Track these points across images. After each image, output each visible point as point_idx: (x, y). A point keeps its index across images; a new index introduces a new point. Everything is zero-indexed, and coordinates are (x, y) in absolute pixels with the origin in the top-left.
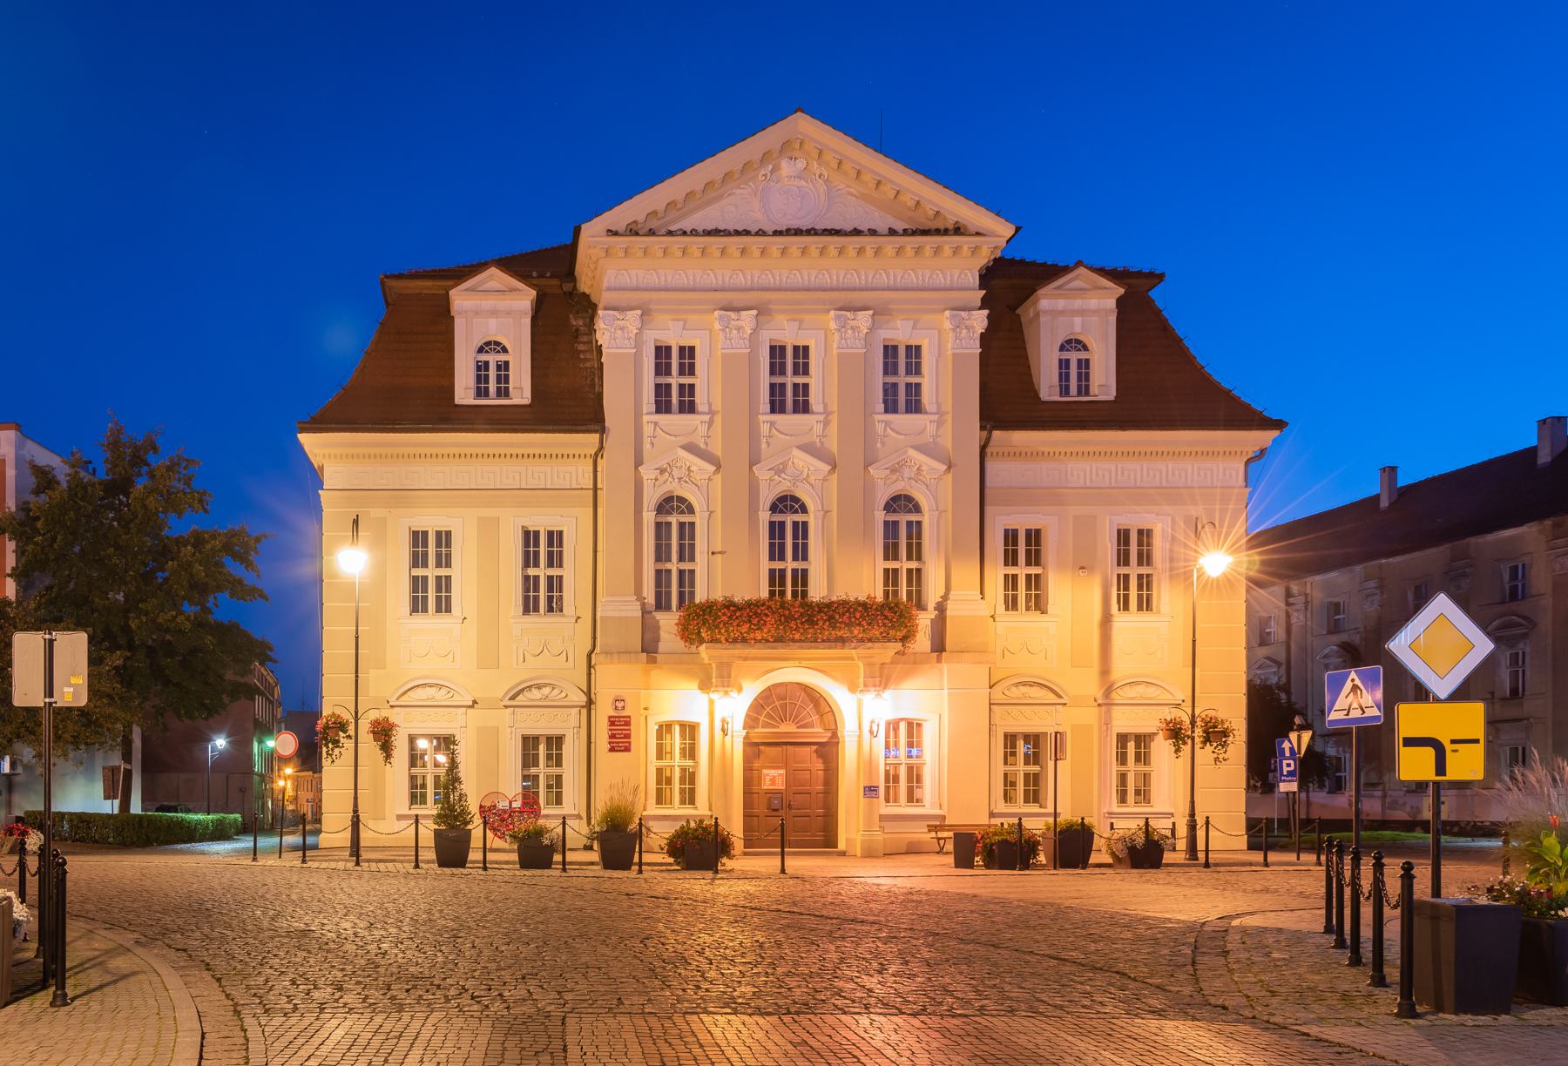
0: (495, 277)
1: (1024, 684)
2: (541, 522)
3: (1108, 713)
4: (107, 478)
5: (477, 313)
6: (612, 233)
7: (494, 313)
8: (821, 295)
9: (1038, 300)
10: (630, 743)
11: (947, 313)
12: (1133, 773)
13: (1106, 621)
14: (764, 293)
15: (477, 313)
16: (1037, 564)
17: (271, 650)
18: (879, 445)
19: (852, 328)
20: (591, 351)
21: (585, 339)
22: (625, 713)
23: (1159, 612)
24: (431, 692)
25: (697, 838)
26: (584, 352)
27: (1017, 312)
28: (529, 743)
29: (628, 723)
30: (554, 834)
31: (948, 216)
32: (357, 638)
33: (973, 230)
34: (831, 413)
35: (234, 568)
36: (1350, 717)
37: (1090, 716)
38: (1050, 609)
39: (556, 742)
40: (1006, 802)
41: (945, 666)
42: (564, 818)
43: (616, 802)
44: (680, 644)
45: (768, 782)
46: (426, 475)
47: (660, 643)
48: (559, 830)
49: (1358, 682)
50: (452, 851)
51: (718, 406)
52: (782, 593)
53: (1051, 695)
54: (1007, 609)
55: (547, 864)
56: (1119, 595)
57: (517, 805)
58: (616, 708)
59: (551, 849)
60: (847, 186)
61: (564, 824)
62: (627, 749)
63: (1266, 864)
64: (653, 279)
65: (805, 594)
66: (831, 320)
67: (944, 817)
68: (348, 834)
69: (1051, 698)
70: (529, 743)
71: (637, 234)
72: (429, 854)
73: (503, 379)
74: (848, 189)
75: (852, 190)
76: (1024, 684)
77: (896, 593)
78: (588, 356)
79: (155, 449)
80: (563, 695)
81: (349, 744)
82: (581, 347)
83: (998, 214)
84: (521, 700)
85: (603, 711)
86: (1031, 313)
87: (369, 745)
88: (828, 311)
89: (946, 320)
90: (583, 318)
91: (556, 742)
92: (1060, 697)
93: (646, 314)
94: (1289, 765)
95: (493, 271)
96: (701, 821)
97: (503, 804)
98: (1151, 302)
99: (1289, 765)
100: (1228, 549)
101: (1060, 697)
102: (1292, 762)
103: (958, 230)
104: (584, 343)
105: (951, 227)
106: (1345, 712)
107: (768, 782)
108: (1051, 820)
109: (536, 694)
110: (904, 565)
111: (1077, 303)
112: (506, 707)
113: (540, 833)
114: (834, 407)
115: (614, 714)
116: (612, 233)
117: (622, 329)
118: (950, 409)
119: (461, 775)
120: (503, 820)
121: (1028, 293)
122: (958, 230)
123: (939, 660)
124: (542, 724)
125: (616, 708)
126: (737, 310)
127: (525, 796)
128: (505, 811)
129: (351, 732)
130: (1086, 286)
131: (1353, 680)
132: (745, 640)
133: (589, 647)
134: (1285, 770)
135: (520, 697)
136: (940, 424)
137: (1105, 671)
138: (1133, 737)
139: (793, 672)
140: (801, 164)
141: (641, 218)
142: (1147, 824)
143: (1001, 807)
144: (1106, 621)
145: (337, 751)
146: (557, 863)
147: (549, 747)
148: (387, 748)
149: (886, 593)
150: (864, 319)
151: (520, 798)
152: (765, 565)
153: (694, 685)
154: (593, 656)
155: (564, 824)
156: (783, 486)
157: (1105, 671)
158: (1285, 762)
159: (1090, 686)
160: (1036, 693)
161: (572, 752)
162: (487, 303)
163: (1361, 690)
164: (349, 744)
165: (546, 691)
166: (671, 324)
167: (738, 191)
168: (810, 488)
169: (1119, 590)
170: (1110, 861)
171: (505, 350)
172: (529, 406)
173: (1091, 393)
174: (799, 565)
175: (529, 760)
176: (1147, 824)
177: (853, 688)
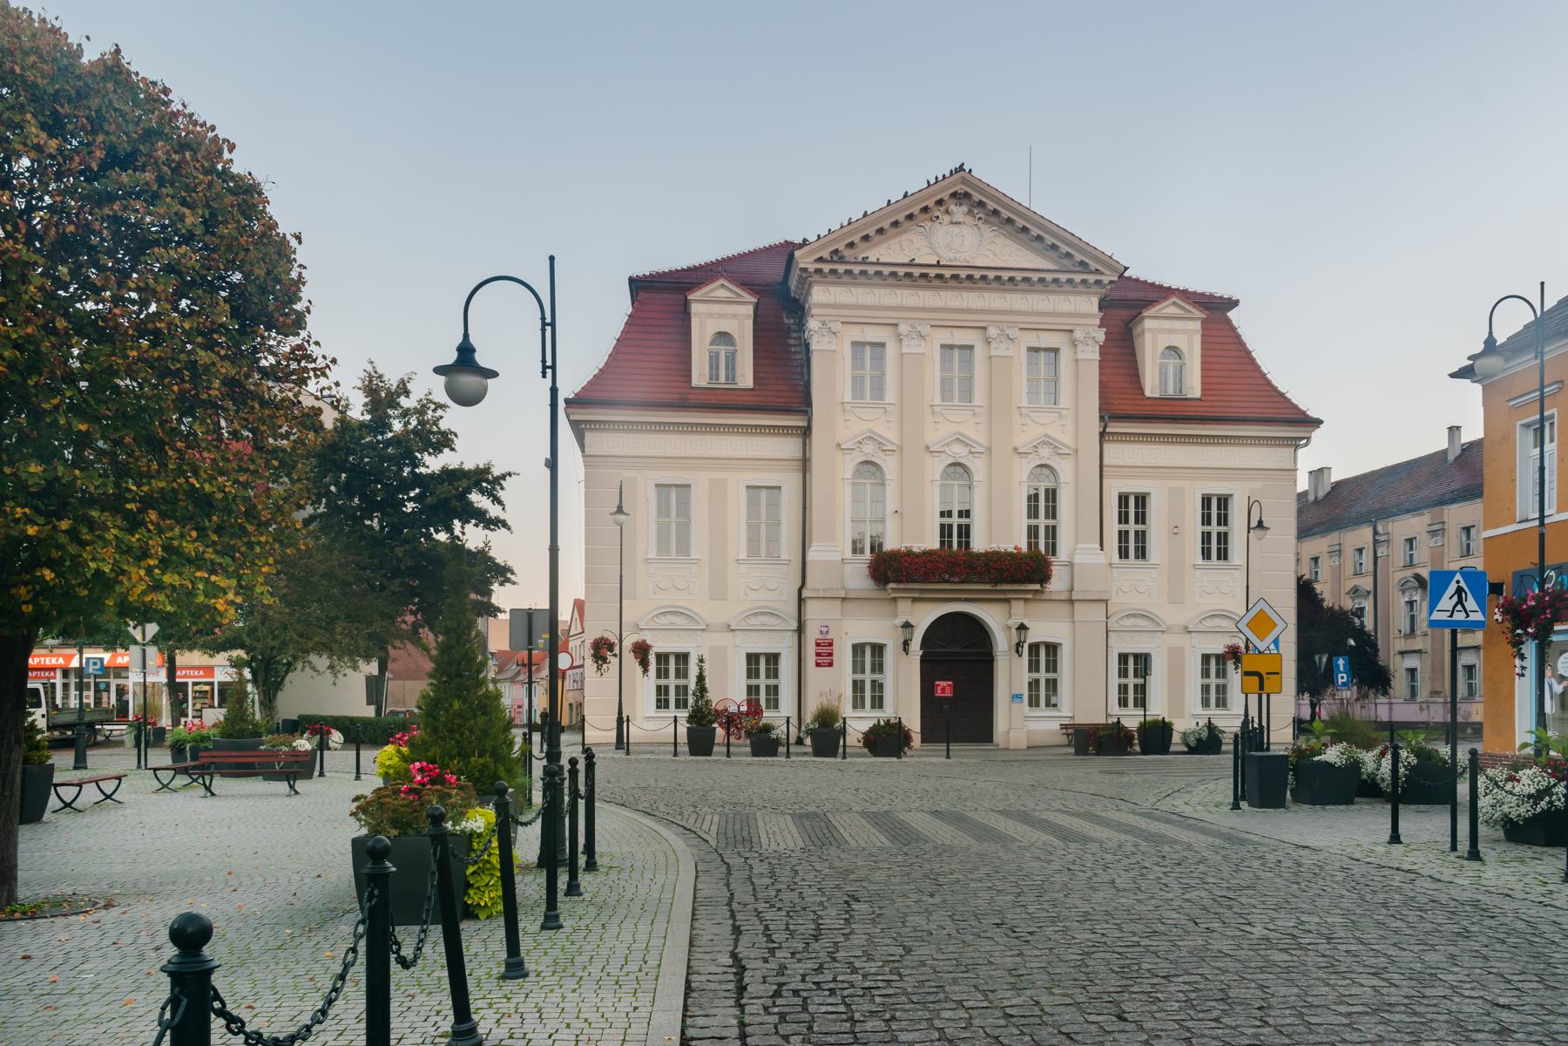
1: (1133, 615)
4: (361, 418)
17: (513, 573)
20: (800, 345)
21: (795, 335)
22: (829, 636)
24: (672, 618)
25: (885, 733)
28: (752, 659)
29: (831, 644)
30: (779, 731)
35: (477, 499)
36: (1477, 609)
39: (773, 659)
40: (1120, 706)
43: (825, 706)
45: (939, 691)
48: (784, 728)
49: (1463, 584)
50: (700, 743)
52: (950, 543)
54: (1121, 557)
55: (774, 753)
57: (744, 709)
58: (821, 632)
59: (777, 742)
62: (831, 665)
65: (968, 544)
68: (614, 733)
70: (752, 659)
72: (684, 748)
76: (1133, 615)
77: (1037, 544)
78: (798, 349)
79: (407, 393)
81: (614, 661)
82: (792, 342)
85: (812, 635)
86: (1139, 330)
87: (630, 660)
91: (773, 659)
94: (1342, 678)
96: (889, 721)
97: (733, 709)
98: (1229, 322)
99: (1342, 678)
102: (1345, 675)
104: (795, 338)
106: (1449, 614)
108: (1142, 719)
113: (768, 729)
119: (707, 685)
121: (1136, 317)
124: (762, 646)
125: (821, 632)
127: (749, 702)
129: (617, 651)
131: (1458, 582)
133: (799, 584)
134: (1340, 681)
142: (1209, 721)
143: (1115, 709)
145: (605, 666)
146: (782, 754)
147: (768, 663)
148: (644, 664)
149: (1029, 544)
151: (745, 703)
154: (803, 591)
158: (1340, 675)
160: (1142, 623)
161: (787, 667)
163: (1466, 593)
164: (614, 661)
170: (1186, 749)
175: (752, 673)
176: (1209, 721)
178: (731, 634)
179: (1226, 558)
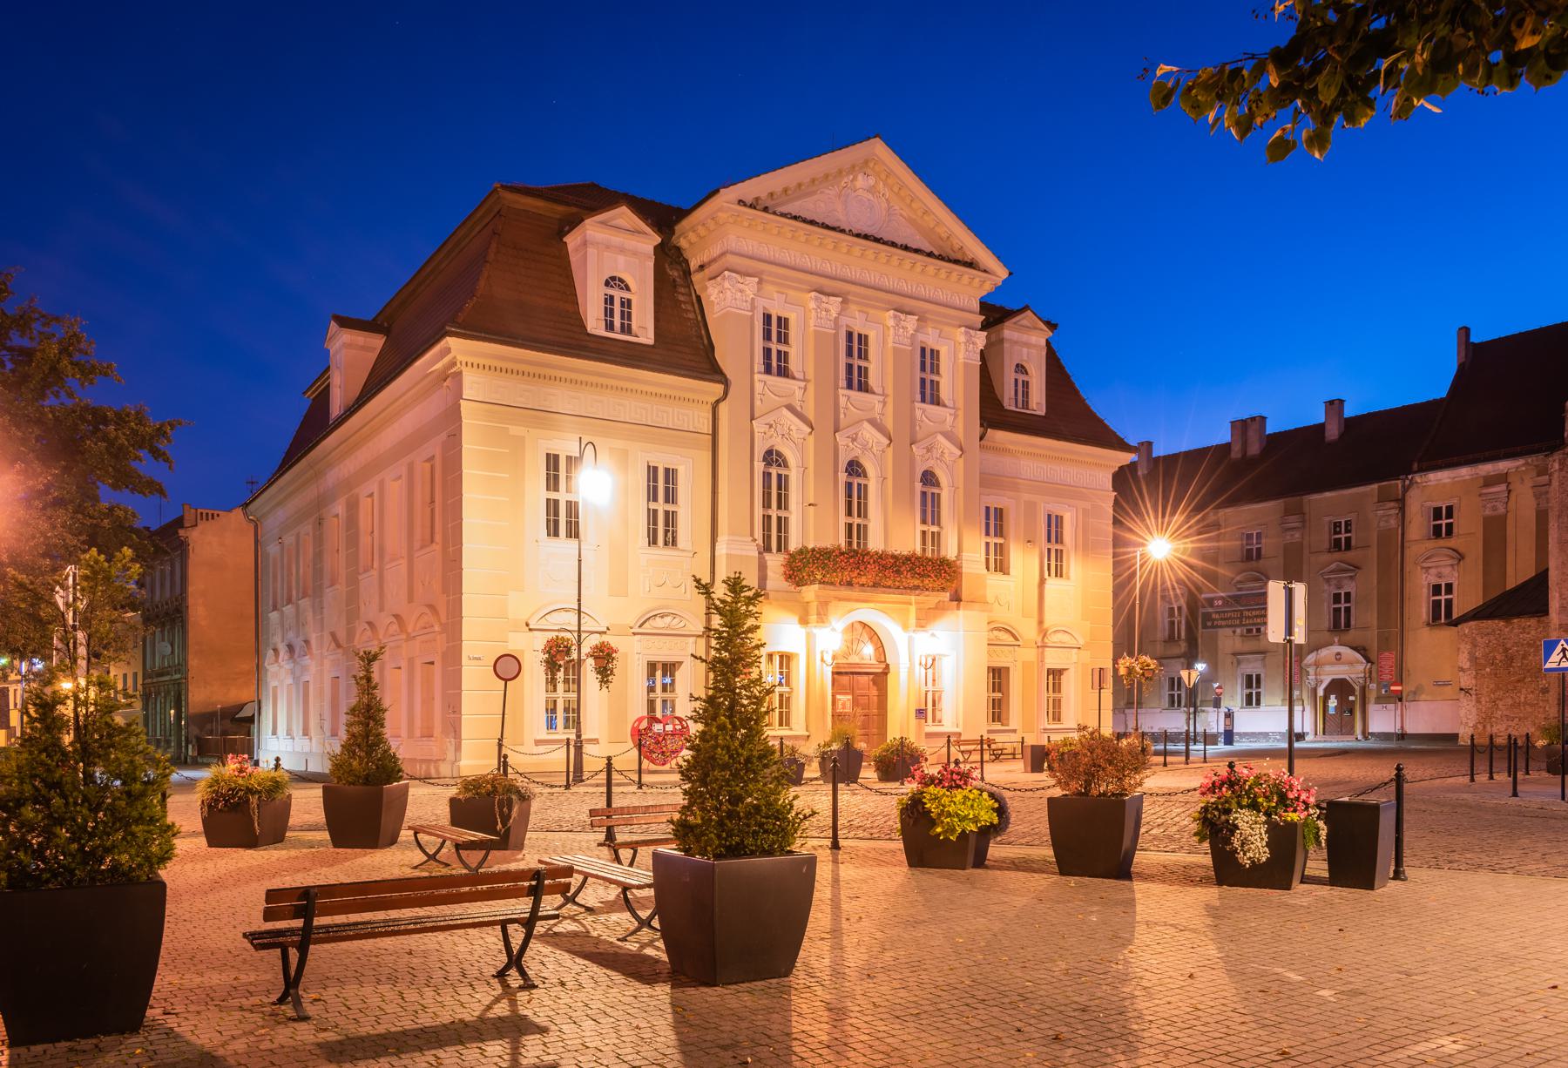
0: (623, 215)
2: (662, 461)
3: (1043, 653)
5: (608, 247)
6: (741, 202)
7: (622, 250)
8: (953, 312)
9: (1003, 329)
11: (963, 329)
13: (1042, 582)
15: (608, 247)
18: (918, 428)
19: (903, 328)
23: (1068, 578)
26: (685, 303)
27: (565, 240)
31: (968, 253)
32: (580, 561)
33: (982, 267)
34: (887, 396)
37: (1030, 654)
38: (1012, 571)
41: (961, 612)
42: (782, 739)
44: (785, 585)
45: (840, 706)
46: (561, 399)
47: (768, 582)
51: (811, 375)
53: (1012, 639)
56: (996, 560)
63: (1165, 764)
64: (765, 251)
65: (865, 544)
66: (889, 318)
67: (960, 734)
69: (1011, 640)
71: (755, 208)
73: (627, 316)
75: (904, 214)
80: (682, 624)
83: (999, 258)
84: (647, 628)
88: (888, 310)
89: (960, 335)
90: (677, 270)
92: (1017, 639)
93: (845, 302)
95: (624, 209)
101: (1017, 639)
103: (971, 265)
107: (840, 706)
109: (659, 622)
110: (856, 521)
111: (1025, 338)
112: (634, 634)
114: (890, 391)
116: (741, 202)
117: (741, 291)
118: (962, 408)
120: (658, 742)
122: (971, 265)
123: (958, 608)
124: (664, 651)
126: (829, 295)
128: (659, 734)
130: (1029, 325)
132: (850, 584)
135: (647, 625)
136: (956, 416)
137: (1041, 622)
138: (661, 666)
139: (867, 613)
140: (872, 181)
141: (763, 195)
144: (1042, 582)
150: (911, 322)
152: (843, 519)
153: (795, 619)
156: (856, 452)
157: (1041, 622)
159: (1028, 630)
162: (617, 239)
165: (668, 620)
166: (775, 295)
167: (827, 191)
168: (945, 467)
169: (996, 555)
171: (628, 289)
172: (653, 346)
173: (1030, 407)
174: (653, 506)
177: (905, 627)
178: (531, 634)
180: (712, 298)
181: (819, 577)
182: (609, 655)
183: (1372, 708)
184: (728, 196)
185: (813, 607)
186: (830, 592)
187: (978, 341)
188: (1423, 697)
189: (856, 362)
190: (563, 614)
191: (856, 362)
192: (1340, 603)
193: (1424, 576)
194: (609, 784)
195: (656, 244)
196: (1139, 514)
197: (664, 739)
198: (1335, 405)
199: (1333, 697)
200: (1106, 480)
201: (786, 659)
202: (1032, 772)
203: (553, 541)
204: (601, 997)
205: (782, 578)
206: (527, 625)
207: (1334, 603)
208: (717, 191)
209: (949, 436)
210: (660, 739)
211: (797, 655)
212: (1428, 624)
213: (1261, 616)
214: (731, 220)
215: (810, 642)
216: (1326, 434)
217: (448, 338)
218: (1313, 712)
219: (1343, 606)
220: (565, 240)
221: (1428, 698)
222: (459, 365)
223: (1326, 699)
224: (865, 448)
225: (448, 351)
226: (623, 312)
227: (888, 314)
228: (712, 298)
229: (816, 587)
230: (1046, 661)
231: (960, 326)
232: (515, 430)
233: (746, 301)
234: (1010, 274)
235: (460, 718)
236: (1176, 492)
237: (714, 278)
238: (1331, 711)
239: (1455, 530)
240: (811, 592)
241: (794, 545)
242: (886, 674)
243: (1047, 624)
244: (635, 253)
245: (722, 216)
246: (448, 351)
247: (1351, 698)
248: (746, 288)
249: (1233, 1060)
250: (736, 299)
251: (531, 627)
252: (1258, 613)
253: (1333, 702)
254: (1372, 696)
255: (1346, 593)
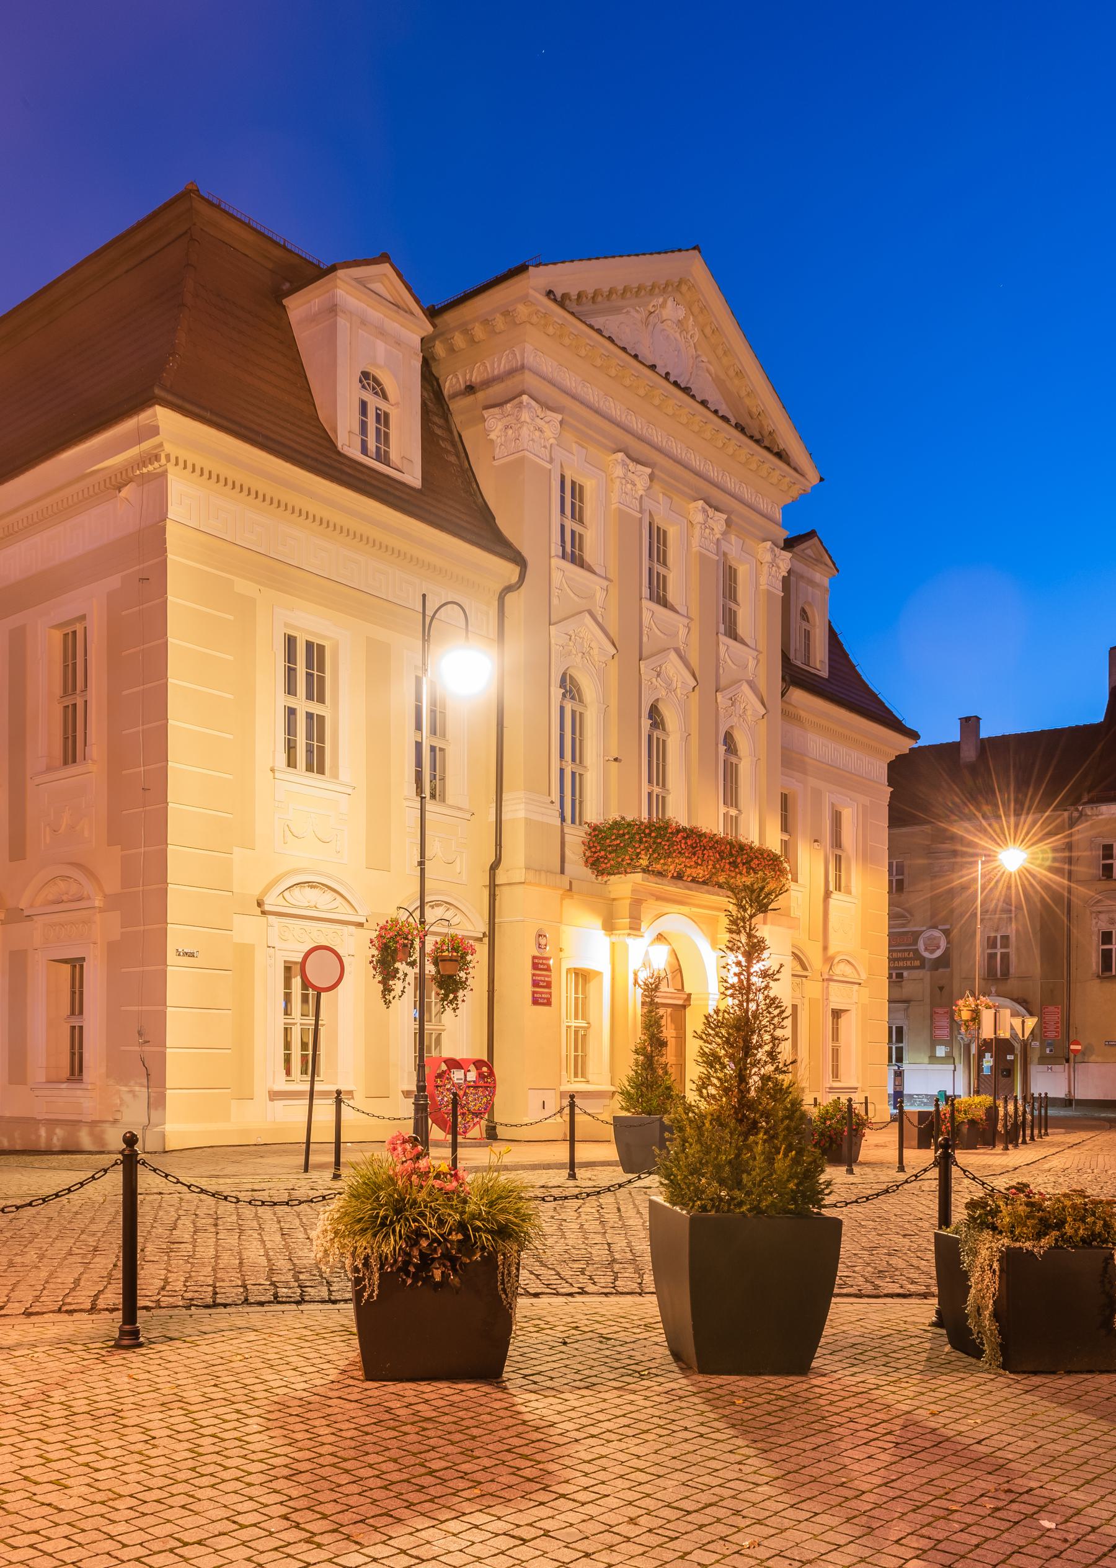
1: (311, 885)
10: (550, 994)
12: (299, 1027)
13: (827, 895)
14: (653, 451)
15: (364, 322)
16: (321, 700)
23: (849, 892)
27: (285, 302)
42: (572, 1097)
60: (709, 362)
61: (572, 1105)
62: (548, 1003)
66: (696, 510)
74: (709, 365)
75: (711, 368)
89: (764, 551)
92: (805, 968)
100: (992, 861)
101: (805, 968)
103: (780, 455)
105: (776, 450)
110: (657, 790)
115: (537, 954)
122: (780, 455)
128: (459, 1087)
132: (679, 877)
144: (827, 895)
152: (645, 788)
153: (598, 922)
155: (572, 1105)
157: (825, 948)
162: (376, 314)
171: (385, 397)
178: (263, 919)
179: (321, 771)
180: (493, 436)
181: (644, 862)
182: (463, 957)
183: (1036, 1070)
184: (538, 278)
185: (624, 907)
186: (654, 885)
187: (781, 564)
188: (1093, 1058)
189: (657, 567)
190: (307, 891)
191: (657, 567)
192: (995, 947)
193: (1094, 921)
194: (338, 1163)
195: (424, 334)
196: (1018, 814)
197: (465, 1094)
198: (970, 724)
199: (988, 1055)
200: (880, 771)
201: (583, 976)
202: (919, 1148)
203: (309, 774)
204: (238, 1485)
205: (582, 862)
206: (259, 904)
207: (1104, 943)
208: (522, 269)
209: (752, 685)
210: (461, 1093)
211: (598, 974)
212: (1098, 976)
213: (898, 959)
214: (535, 319)
215: (617, 956)
216: (962, 755)
217: (158, 408)
218: (967, 1072)
219: (999, 951)
220: (285, 302)
221: (1099, 1059)
222: (163, 461)
223: (981, 1056)
224: (670, 688)
225: (154, 431)
226: (378, 430)
227: (693, 505)
228: (493, 436)
229: (638, 877)
230: (831, 998)
231: (765, 540)
232: (243, 586)
233: (545, 447)
234: (822, 480)
235: (164, 1054)
236: (1045, 789)
237: (500, 405)
238: (987, 1072)
239: (906, 885)
240: (623, 885)
241: (593, 814)
242: (684, 1007)
243: (831, 951)
244: (398, 343)
245: (522, 310)
246: (154, 431)
247: (1010, 1057)
248: (546, 427)
249: (313, 1436)
250: (533, 440)
251: (267, 908)
252: (900, 955)
253: (988, 1062)
254: (1035, 1056)
255: (1001, 936)
